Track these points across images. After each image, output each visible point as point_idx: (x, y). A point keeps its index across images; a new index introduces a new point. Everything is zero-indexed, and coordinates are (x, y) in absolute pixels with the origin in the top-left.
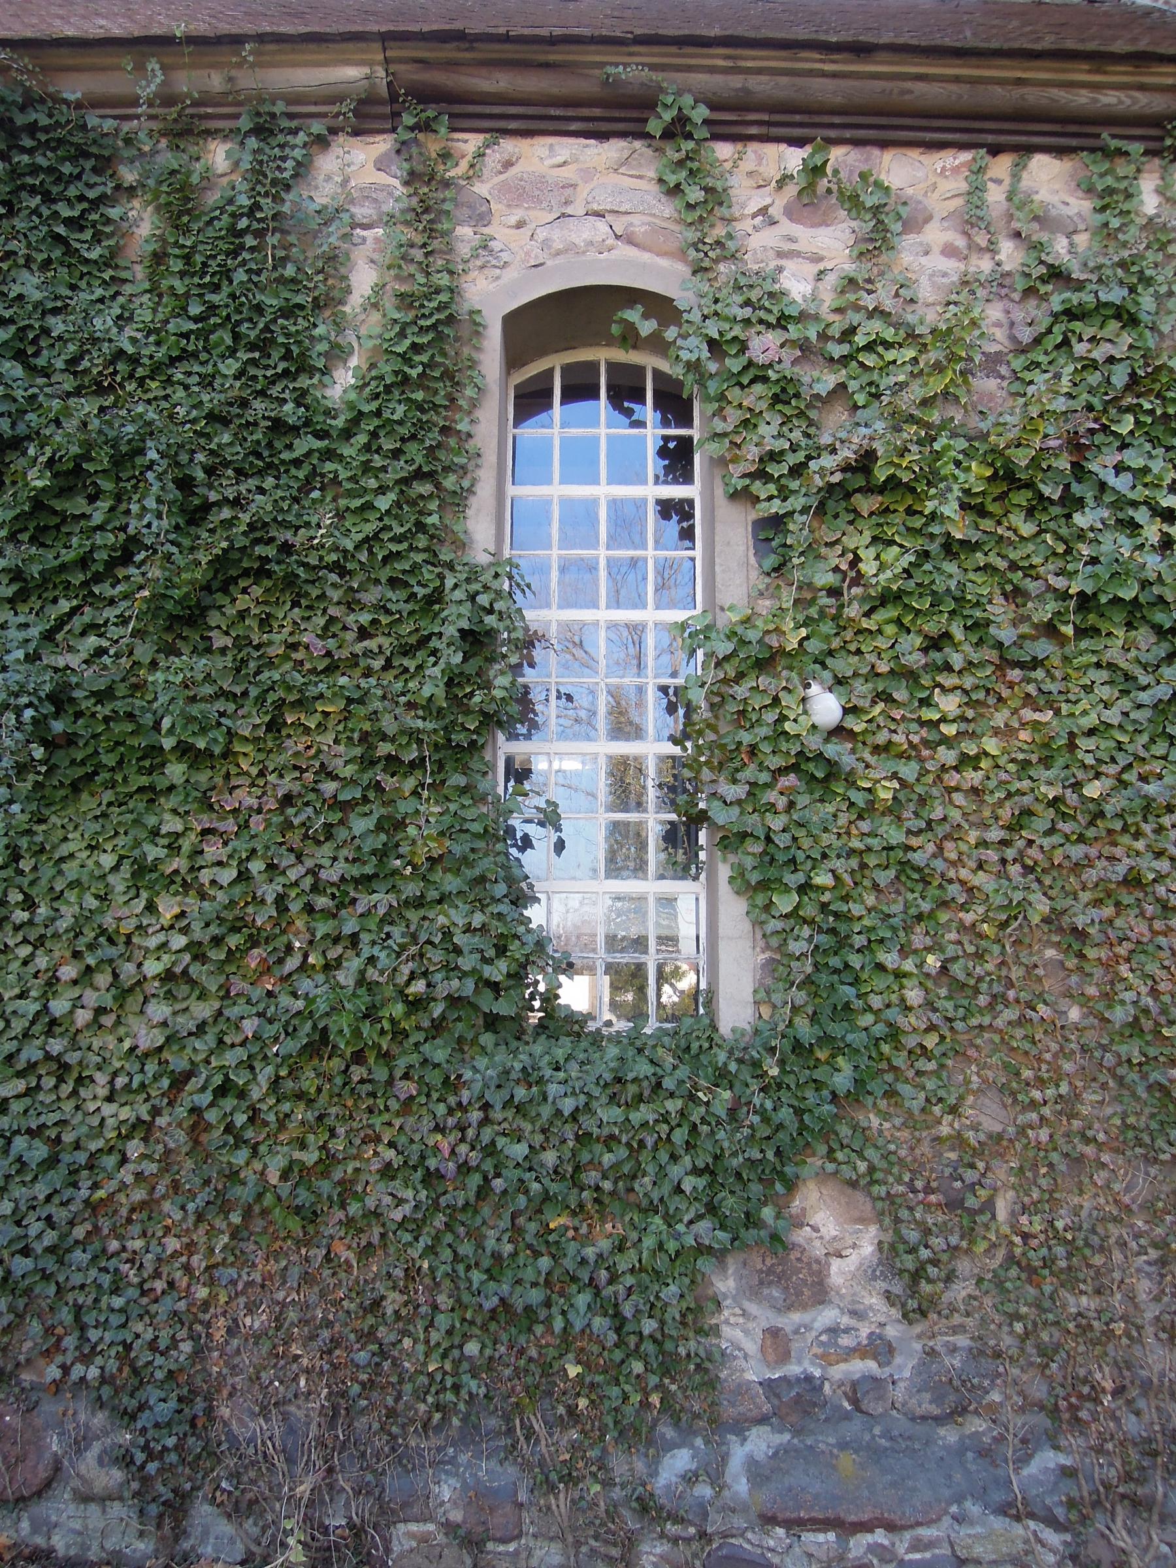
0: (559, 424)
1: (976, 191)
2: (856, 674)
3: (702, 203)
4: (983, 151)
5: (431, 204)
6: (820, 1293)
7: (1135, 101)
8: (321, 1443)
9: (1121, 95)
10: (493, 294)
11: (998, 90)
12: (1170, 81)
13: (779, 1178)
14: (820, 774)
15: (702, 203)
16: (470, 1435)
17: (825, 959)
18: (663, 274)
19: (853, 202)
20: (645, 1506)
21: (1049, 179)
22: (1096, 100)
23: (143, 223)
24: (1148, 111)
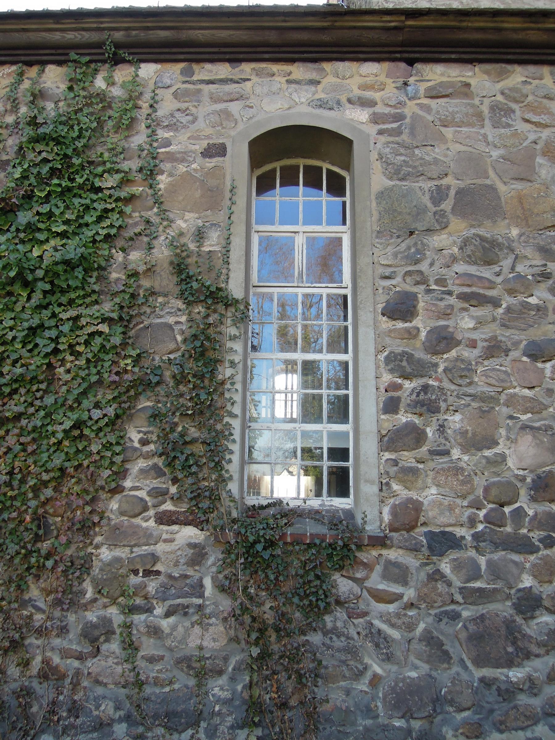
0: (278, 196)
2: (124, 333)
4: (20, 65)
7: (83, 36)
8: (64, 687)
9: (76, 34)
11: (17, 34)
12: (552, 26)
22: (64, 37)
24: (91, 41)
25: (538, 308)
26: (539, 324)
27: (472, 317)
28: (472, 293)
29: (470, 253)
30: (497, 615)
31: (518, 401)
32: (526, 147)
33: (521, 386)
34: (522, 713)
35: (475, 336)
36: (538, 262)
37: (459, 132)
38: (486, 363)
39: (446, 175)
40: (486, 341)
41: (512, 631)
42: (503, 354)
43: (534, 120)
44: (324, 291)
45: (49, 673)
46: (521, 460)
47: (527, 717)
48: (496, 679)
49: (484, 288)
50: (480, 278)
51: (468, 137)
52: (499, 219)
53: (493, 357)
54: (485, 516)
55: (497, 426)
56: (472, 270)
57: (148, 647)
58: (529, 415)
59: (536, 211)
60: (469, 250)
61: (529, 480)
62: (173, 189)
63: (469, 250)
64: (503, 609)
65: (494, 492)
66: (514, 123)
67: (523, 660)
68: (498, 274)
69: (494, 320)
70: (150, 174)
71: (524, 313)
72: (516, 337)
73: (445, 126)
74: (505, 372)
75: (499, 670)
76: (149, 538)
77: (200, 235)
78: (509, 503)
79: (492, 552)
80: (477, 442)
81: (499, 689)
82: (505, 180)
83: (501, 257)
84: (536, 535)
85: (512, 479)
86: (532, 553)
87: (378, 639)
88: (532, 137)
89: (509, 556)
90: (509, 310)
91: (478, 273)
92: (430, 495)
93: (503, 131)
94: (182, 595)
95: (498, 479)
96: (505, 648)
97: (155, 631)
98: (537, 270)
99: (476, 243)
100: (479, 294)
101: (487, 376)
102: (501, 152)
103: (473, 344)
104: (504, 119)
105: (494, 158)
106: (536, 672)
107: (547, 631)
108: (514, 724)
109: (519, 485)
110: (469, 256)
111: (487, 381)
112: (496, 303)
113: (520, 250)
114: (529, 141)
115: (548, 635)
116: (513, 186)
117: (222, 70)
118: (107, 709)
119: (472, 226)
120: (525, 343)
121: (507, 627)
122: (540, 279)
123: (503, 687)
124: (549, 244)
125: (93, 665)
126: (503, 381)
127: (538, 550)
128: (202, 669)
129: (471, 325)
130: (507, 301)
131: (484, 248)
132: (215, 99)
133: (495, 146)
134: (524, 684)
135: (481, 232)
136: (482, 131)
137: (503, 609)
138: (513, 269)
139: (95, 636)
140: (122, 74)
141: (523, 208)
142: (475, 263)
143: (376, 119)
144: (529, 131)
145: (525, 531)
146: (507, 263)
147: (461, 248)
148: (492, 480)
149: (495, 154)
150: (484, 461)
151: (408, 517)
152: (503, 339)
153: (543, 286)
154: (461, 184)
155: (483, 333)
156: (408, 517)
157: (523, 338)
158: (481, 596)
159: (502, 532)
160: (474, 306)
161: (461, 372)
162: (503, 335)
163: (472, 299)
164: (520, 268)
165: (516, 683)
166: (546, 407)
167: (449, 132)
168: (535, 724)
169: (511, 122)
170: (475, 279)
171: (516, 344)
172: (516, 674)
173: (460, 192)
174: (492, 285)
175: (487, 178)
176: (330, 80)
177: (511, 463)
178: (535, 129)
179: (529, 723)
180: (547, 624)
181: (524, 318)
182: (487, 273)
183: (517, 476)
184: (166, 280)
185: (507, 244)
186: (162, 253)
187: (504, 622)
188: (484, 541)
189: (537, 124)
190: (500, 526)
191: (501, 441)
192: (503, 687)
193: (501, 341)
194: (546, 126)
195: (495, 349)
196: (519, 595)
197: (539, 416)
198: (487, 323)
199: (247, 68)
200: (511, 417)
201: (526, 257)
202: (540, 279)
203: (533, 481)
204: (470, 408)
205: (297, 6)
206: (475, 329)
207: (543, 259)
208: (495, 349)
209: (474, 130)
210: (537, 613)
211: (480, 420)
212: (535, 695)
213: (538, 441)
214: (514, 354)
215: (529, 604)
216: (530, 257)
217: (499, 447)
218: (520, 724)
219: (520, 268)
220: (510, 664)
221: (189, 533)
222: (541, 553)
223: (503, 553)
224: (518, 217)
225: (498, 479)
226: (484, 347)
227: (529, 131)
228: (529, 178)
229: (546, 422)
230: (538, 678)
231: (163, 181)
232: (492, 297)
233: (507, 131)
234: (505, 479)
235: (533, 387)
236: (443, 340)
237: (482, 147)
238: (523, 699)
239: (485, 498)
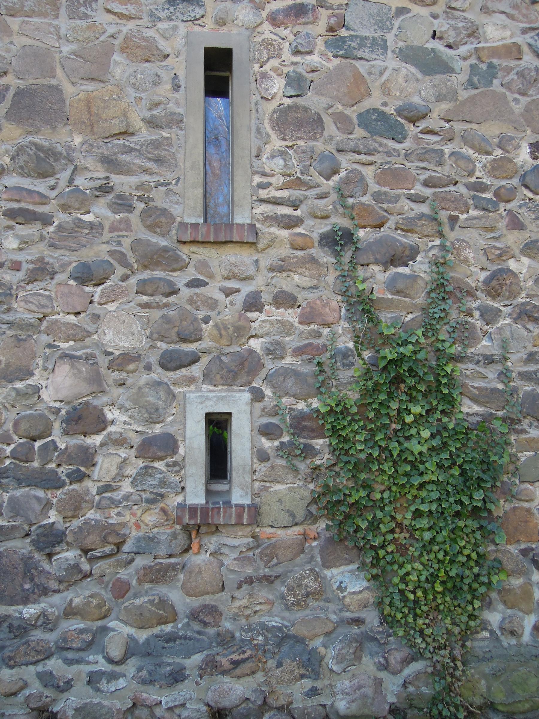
19: (370, 320)
25: (92, 226)
26: (92, 244)
27: (17, 236)
28: (20, 209)
29: (22, 164)
30: (15, 552)
31: (59, 328)
32: (102, 42)
33: (64, 312)
34: (33, 648)
35: (20, 257)
36: (101, 174)
37: (27, 23)
38: (29, 287)
39: (5, 73)
40: (32, 263)
42: (48, 278)
43: (117, 10)
46: (57, 390)
47: (38, 652)
48: (9, 616)
49: (34, 203)
50: (30, 192)
51: (37, 29)
52: (60, 126)
53: (36, 280)
54: (12, 452)
55: (34, 356)
56: (26, 183)
58: (71, 343)
59: (104, 116)
60: (22, 160)
61: (63, 412)
63: (22, 160)
65: (23, 426)
66: (93, 14)
67: (40, 596)
68: (53, 188)
69: (42, 238)
71: (76, 232)
72: (66, 258)
73: (12, 16)
74: (49, 297)
75: (13, 607)
78: (40, 437)
79: (16, 489)
81: (10, 626)
82: (73, 80)
83: (57, 168)
84: (63, 471)
85: (46, 412)
86: (58, 488)
88: (111, 30)
89: (33, 492)
90: (60, 228)
91: (31, 187)
93: (78, 22)
95: (31, 412)
96: (22, 585)
98: (98, 183)
99: (31, 153)
100: (27, 210)
101: (26, 302)
102: (74, 47)
103: (16, 266)
104: (82, 9)
105: (64, 54)
106: (52, 607)
107: (66, 567)
108: (23, 660)
109: (52, 417)
110: (21, 167)
111: (26, 307)
112: (46, 220)
113: (81, 160)
114: (107, 34)
115: (66, 570)
116: (83, 87)
119: (28, 133)
120: (74, 264)
121: (26, 565)
122: (97, 193)
123: (16, 623)
124: (115, 154)
126: (43, 306)
127: (63, 485)
129: (15, 245)
130: (60, 218)
131: (38, 157)
133: (68, 41)
134: (37, 619)
135: (38, 139)
136: (56, 22)
138: (71, 181)
141: (90, 113)
142: (29, 176)
144: (110, 23)
145: (53, 466)
146: (65, 176)
147: (13, 159)
148: (23, 413)
149: (66, 49)
150: (13, 394)
152: (51, 261)
153: (102, 201)
154: (22, 84)
155: (29, 254)
157: (73, 259)
159: (28, 467)
160: (20, 224)
162: (51, 256)
164: (79, 181)
165: (29, 619)
166: (90, 334)
167: (14, 23)
168: (48, 658)
169: (89, 13)
170: (25, 193)
171: (64, 266)
172: (29, 611)
173: (20, 93)
174: (44, 200)
175: (54, 77)
177: (45, 395)
178: (119, 21)
179: (40, 657)
180: (67, 560)
181: (76, 237)
183: (50, 408)
185: (65, 154)
187: (22, 559)
188: (7, 478)
189: (120, 16)
190: (27, 462)
191: (37, 372)
192: (16, 623)
193: (48, 263)
194: (130, 18)
195: (41, 271)
196: (38, 531)
197: (82, 344)
198: (34, 243)
200: (50, 346)
201: (86, 168)
202: (97, 193)
203: (68, 413)
204: (4, 336)
206: (21, 249)
207: (107, 171)
208: (41, 271)
209: (46, 20)
210: (58, 549)
211: (16, 349)
212: (51, 630)
213: (76, 371)
214: (60, 277)
216: (91, 168)
217: (35, 378)
218: (30, 659)
219: (79, 181)
220: (25, 601)
222: (67, 487)
223: (27, 489)
224: (84, 123)
225: (31, 412)
226: (28, 269)
227: (110, 23)
228: (101, 78)
229: (89, 351)
230: (53, 613)
232: (44, 214)
233: (84, 23)
234: (37, 412)
235: (79, 313)
237: (52, 41)
238: (37, 635)
239: (15, 432)
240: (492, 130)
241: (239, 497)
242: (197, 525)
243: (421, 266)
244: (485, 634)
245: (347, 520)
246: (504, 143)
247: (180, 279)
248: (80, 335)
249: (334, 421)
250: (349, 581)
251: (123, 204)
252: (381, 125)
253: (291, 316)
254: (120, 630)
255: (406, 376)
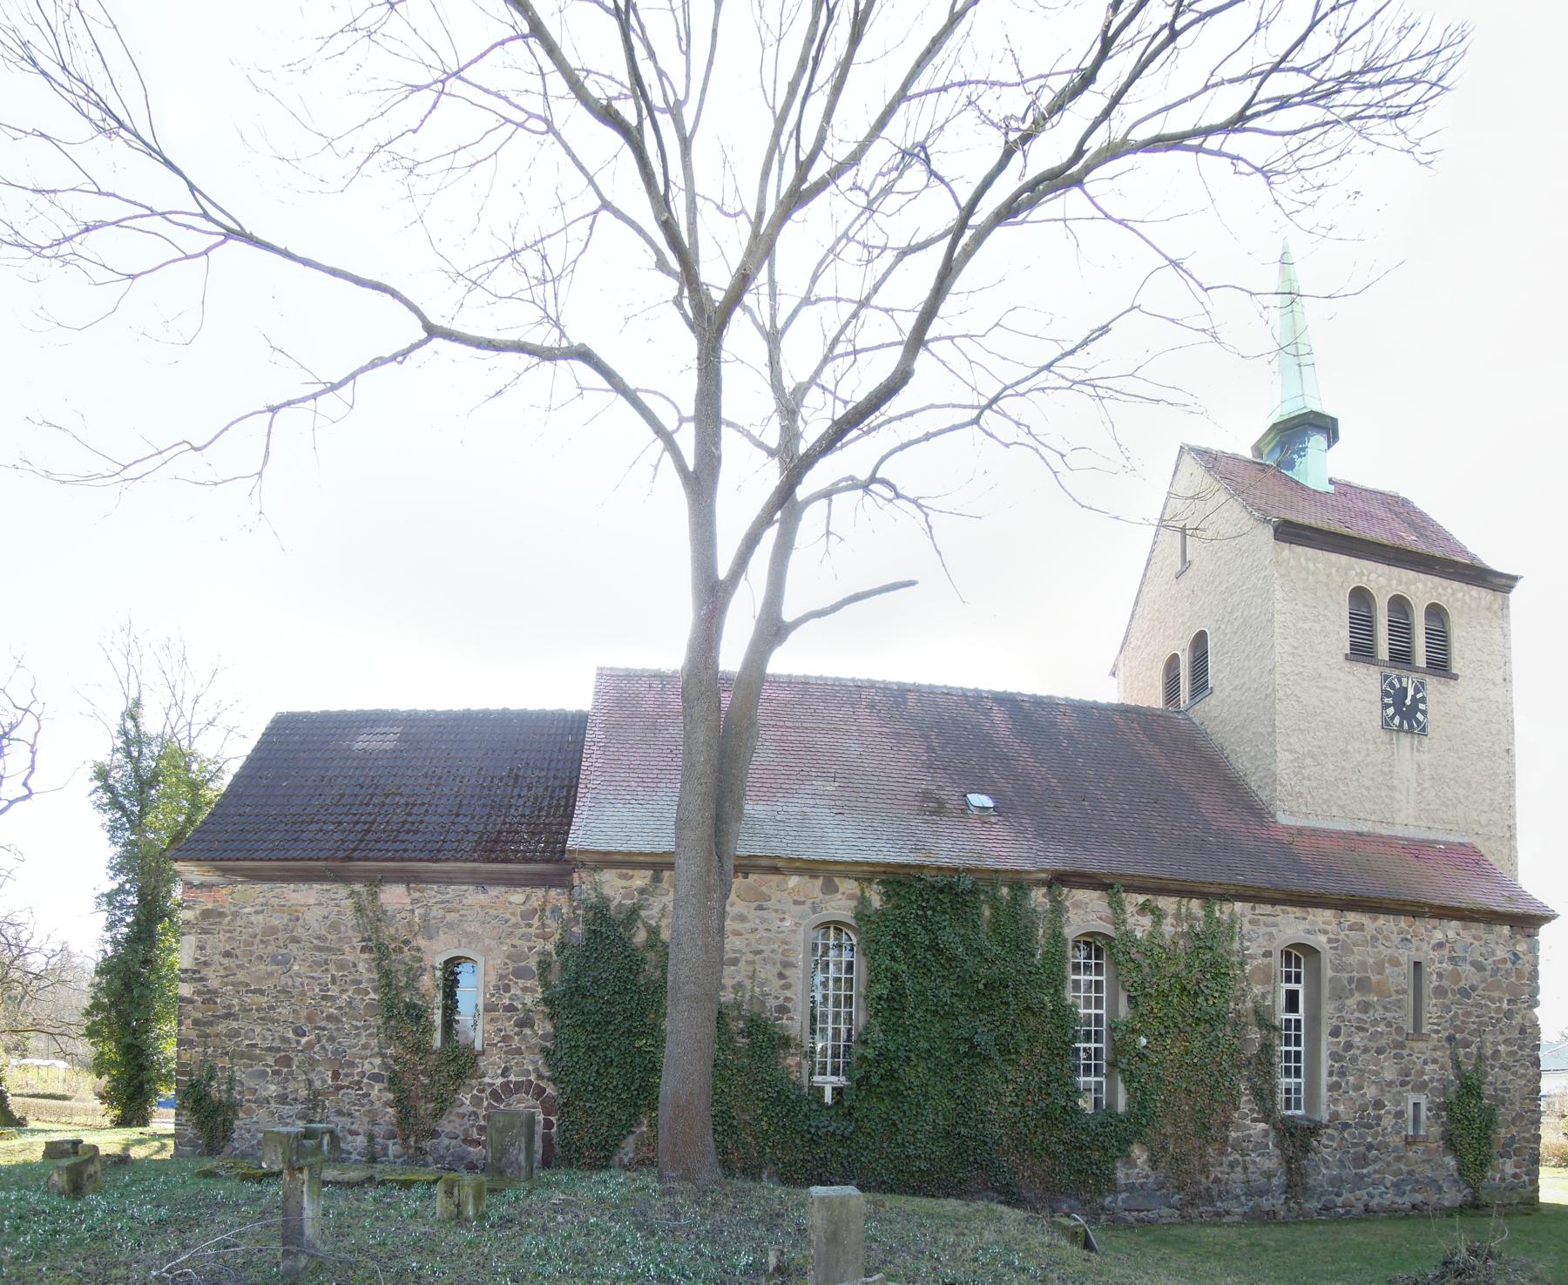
1: (1179, 909)
3: (1117, 906)
5: (1058, 910)
6: (1136, 1166)
10: (1070, 932)
13: (1130, 1142)
14: (1142, 1056)
15: (1117, 906)
16: (1069, 1196)
17: (1140, 1101)
18: (1108, 929)
19: (1153, 912)
20: (1103, 1209)
21: (1195, 905)
23: (987, 912)
41: (1364, 1157)
44: (1292, 1016)
45: (1217, 1181)
57: (1252, 1168)
62: (1252, 972)
64: (1362, 1149)
70: (1242, 964)
76: (1249, 1128)
77: (1264, 996)
80: (1358, 1088)
87: (1325, 1161)
92: (1341, 1108)
94: (1261, 1147)
97: (1254, 1162)
117: (1268, 909)
118: (1238, 1191)
125: (1233, 1176)
128: (1269, 1175)
132: (1265, 925)
137: (1362, 1149)
139: (1232, 1166)
140: (1227, 907)
143: (1330, 941)
151: (1335, 1116)
156: (1335, 1116)
158: (1356, 1145)
161: (1354, 1060)
163: (1360, 1029)
176: (1310, 917)
182: (1364, 1017)
184: (1252, 1018)
186: (1249, 1005)
195: (1366, 1050)
199: (1278, 908)
205: (416, 712)
208: (1366, 1050)
215: (1370, 1147)
221: (1262, 1125)
231: (1248, 968)
236: (1349, 1046)
240: (1496, 994)
241: (1422, 1132)
242: (1410, 1142)
243: (1473, 1049)
244: (1038, 897)
245: (1450, 1143)
246: (1500, 1000)
247: (1405, 1053)
248: (1377, 1074)
249: (1448, 1107)
250: (1450, 1161)
251: (1389, 1025)
252: (1465, 993)
253: (1436, 1067)
254: (1389, 1178)
255: (1469, 1088)
